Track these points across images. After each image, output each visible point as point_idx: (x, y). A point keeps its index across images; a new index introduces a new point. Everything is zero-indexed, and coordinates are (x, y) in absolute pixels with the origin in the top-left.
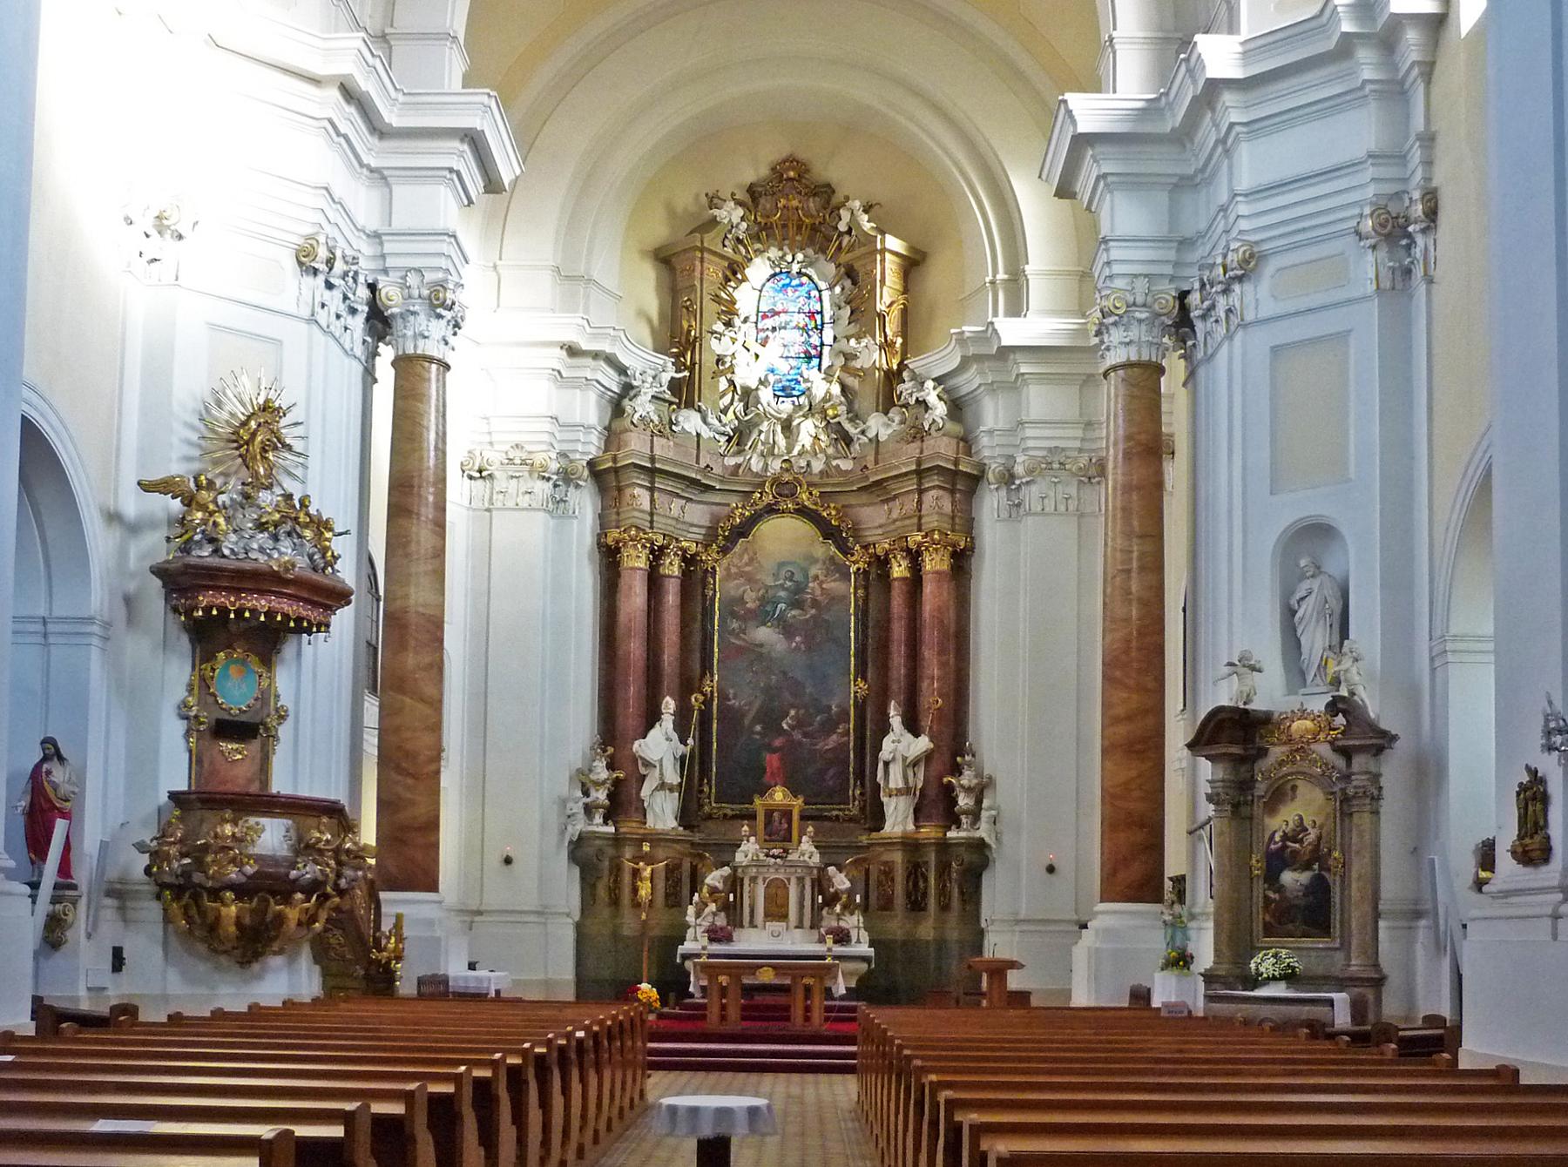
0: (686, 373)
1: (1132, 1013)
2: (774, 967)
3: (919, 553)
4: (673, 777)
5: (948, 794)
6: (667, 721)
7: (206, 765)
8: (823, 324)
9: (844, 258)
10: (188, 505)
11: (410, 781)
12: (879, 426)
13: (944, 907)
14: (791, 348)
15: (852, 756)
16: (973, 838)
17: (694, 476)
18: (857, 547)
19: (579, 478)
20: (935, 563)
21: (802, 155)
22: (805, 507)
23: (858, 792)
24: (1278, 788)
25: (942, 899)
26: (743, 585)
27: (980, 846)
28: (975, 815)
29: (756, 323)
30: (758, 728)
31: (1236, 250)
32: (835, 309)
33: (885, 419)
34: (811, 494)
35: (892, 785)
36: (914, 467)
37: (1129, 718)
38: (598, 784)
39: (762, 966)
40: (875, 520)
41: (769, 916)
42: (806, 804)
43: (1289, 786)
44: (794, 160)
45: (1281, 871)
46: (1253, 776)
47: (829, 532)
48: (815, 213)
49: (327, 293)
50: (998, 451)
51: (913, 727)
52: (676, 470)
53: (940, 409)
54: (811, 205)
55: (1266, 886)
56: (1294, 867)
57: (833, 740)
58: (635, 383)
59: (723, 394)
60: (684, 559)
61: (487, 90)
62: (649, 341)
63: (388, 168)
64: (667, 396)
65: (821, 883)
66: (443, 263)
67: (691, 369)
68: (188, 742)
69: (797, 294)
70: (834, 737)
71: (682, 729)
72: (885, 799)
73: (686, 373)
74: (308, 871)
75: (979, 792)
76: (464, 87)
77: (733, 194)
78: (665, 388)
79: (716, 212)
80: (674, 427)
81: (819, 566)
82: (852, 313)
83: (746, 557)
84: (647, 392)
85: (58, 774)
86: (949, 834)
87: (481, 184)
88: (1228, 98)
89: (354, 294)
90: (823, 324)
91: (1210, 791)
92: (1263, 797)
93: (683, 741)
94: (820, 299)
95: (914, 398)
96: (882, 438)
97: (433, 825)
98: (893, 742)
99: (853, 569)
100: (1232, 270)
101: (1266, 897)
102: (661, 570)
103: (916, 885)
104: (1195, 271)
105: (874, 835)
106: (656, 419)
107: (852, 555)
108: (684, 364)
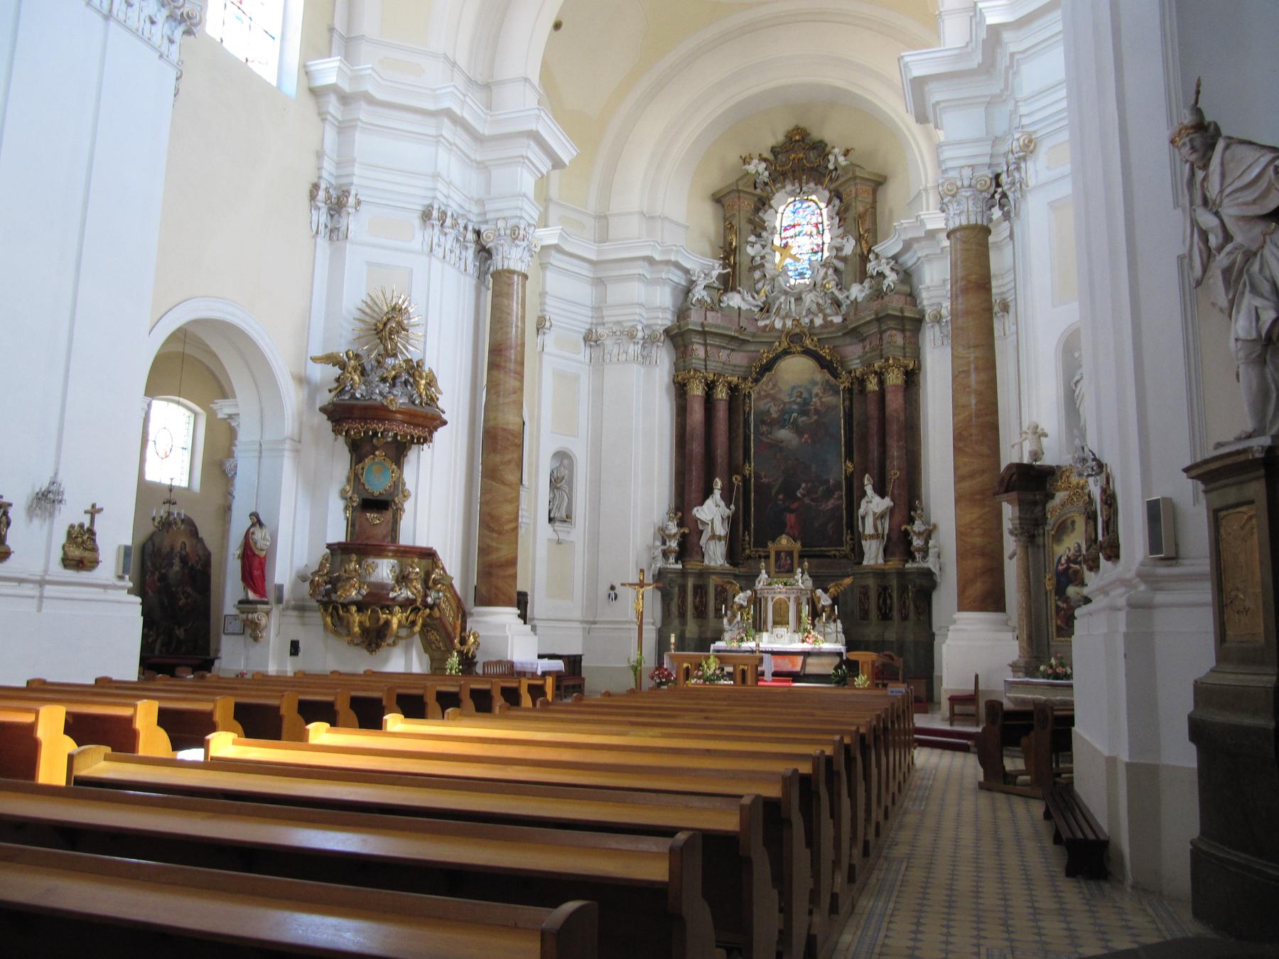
0: (729, 270)
1: (867, 692)
4: (721, 530)
5: (906, 538)
7: (357, 527)
8: (823, 230)
9: (833, 186)
11: (495, 535)
12: (857, 291)
13: (905, 618)
17: (733, 334)
18: (844, 373)
19: (658, 341)
20: (894, 378)
21: (802, 125)
24: (1060, 525)
25: (903, 611)
26: (769, 403)
27: (928, 574)
28: (925, 551)
30: (781, 497)
31: (1018, 139)
34: (812, 340)
35: (866, 532)
36: (873, 317)
37: (971, 476)
38: (671, 537)
40: (854, 354)
43: (1069, 522)
45: (1067, 585)
46: (1045, 515)
48: (813, 159)
49: (443, 239)
50: (933, 301)
51: (881, 492)
53: (891, 278)
55: (1057, 598)
56: (1077, 583)
57: (831, 504)
58: (694, 278)
59: (759, 281)
60: (730, 388)
63: (490, 160)
64: (715, 285)
65: (813, 603)
67: (734, 267)
68: (346, 513)
69: (806, 213)
70: (832, 501)
71: (727, 498)
73: (729, 270)
74: (406, 593)
75: (928, 535)
77: (760, 155)
78: (714, 279)
79: (747, 167)
81: (820, 386)
82: (840, 221)
85: (259, 535)
86: (907, 566)
87: (549, 164)
88: (1007, 36)
90: (823, 230)
93: (728, 506)
94: (821, 214)
96: (859, 300)
99: (842, 386)
100: (1017, 153)
101: (1057, 607)
102: (715, 397)
103: (885, 601)
105: (856, 567)
106: (709, 300)
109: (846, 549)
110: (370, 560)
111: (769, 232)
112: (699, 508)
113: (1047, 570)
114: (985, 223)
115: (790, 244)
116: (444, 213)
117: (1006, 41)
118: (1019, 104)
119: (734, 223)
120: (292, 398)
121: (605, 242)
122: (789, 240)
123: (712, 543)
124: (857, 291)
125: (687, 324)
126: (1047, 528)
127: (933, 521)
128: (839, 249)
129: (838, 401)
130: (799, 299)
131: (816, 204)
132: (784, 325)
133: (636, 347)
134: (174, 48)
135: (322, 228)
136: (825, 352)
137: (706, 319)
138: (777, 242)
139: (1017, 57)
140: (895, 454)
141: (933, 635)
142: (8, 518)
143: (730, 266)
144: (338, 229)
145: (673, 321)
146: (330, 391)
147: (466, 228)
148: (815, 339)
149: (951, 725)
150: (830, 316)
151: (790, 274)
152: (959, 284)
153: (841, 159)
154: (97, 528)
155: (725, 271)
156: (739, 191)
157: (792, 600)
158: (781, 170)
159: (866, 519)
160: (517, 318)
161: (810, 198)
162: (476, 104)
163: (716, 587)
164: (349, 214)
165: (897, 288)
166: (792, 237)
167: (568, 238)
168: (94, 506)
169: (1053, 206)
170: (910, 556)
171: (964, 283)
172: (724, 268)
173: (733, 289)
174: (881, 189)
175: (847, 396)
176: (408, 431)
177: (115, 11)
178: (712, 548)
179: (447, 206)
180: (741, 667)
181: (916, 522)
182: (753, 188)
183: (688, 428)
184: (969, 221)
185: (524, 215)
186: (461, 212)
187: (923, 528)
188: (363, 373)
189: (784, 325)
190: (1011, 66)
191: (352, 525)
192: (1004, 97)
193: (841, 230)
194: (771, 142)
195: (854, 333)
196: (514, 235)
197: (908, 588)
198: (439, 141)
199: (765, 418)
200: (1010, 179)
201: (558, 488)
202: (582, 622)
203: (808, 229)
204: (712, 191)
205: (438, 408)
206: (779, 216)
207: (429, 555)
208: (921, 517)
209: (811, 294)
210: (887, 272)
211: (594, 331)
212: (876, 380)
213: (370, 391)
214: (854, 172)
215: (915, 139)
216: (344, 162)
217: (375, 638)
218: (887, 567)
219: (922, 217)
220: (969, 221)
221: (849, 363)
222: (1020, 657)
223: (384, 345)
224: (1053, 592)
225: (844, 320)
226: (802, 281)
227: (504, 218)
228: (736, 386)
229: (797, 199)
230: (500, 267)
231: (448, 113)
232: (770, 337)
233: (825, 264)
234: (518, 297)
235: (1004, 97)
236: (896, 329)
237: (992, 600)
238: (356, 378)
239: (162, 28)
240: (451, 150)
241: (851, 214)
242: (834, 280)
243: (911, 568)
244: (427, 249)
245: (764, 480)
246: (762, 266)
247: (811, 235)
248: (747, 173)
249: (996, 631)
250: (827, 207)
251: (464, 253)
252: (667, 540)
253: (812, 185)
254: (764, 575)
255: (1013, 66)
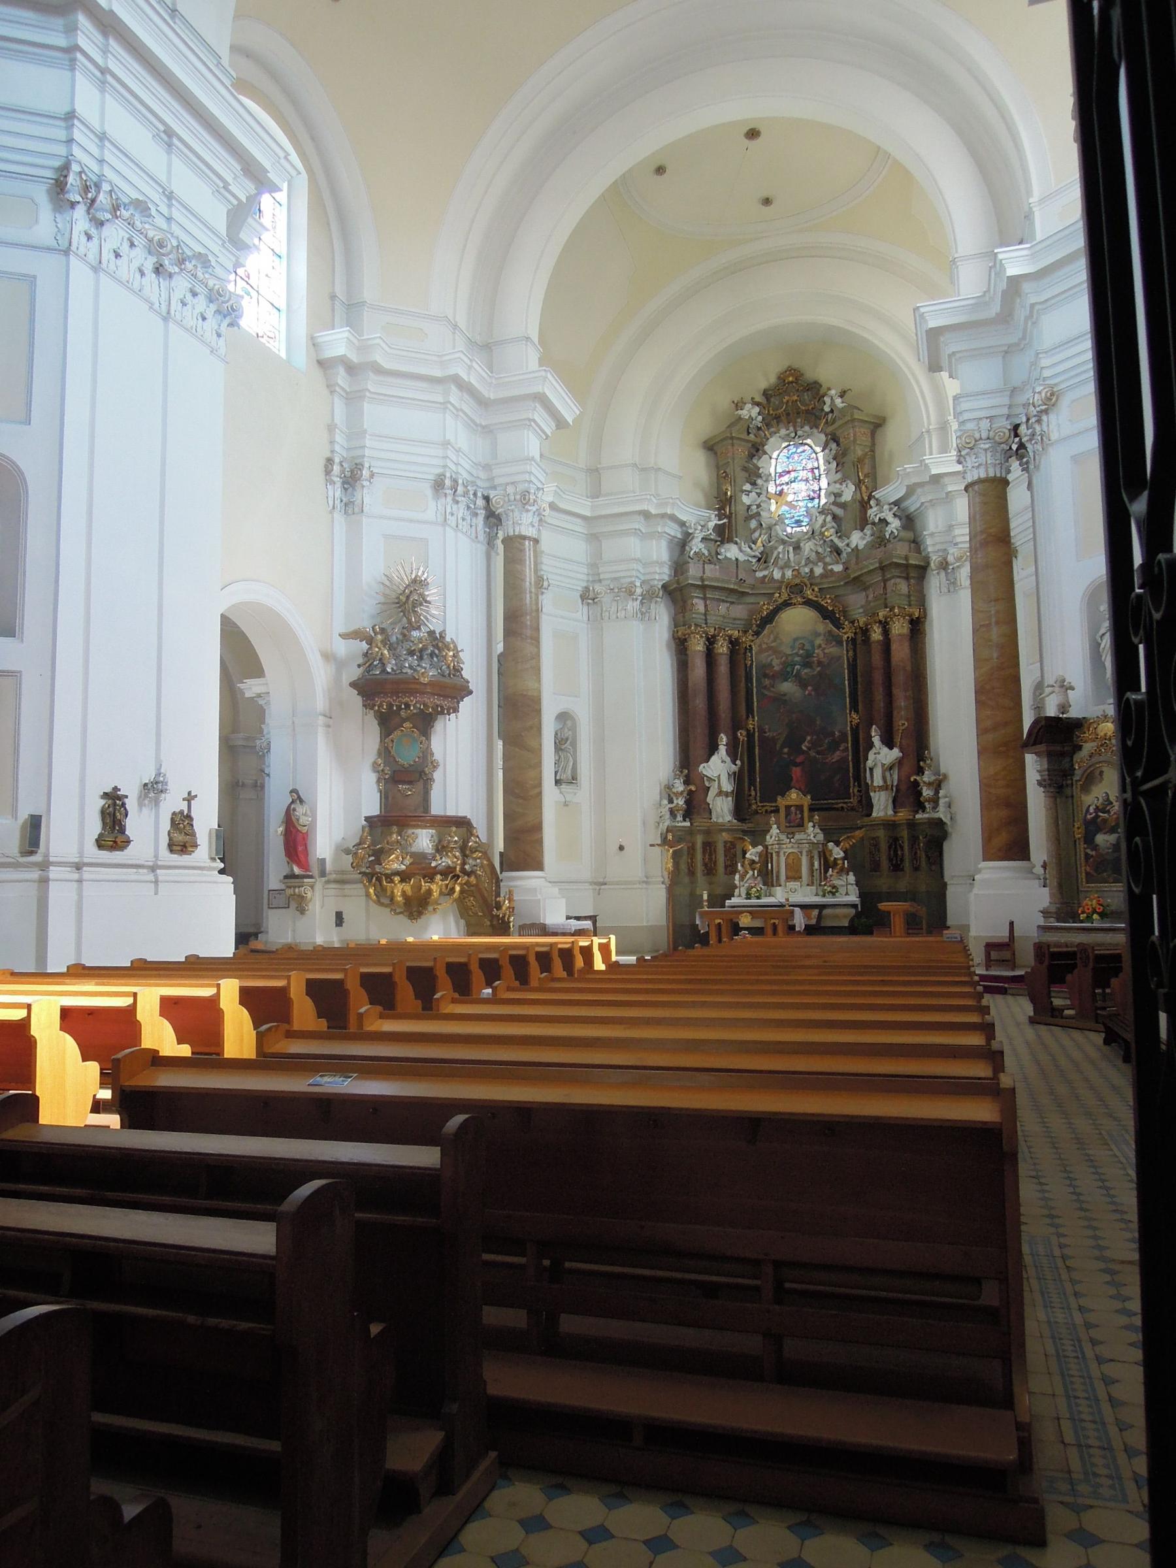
0: (725, 521)
2: (750, 912)
3: (887, 623)
4: (728, 786)
6: (722, 749)
7: (390, 799)
8: (820, 476)
9: (830, 429)
10: (370, 644)
11: (521, 801)
12: (858, 539)
14: (800, 495)
15: (851, 766)
16: (933, 819)
17: (732, 587)
18: (846, 623)
19: (657, 597)
20: (899, 628)
21: (795, 366)
22: (811, 600)
23: (856, 790)
24: (1088, 775)
26: (769, 656)
27: (940, 823)
28: (935, 801)
29: (775, 481)
30: (786, 750)
31: (1040, 393)
32: (827, 464)
33: (861, 534)
34: (813, 590)
35: (875, 784)
36: (877, 565)
39: (742, 912)
40: (856, 603)
41: (788, 878)
42: (812, 800)
44: (792, 369)
45: (1095, 835)
46: (1073, 765)
47: (826, 614)
48: (808, 402)
49: (455, 507)
50: (938, 547)
51: (889, 743)
52: (719, 585)
53: (895, 524)
54: (806, 397)
55: (1085, 846)
57: (837, 756)
58: (690, 531)
59: (754, 531)
60: (731, 642)
61: (544, 368)
62: (703, 503)
63: (496, 424)
64: (712, 537)
65: (824, 855)
66: (527, 477)
67: (729, 517)
68: (379, 785)
69: (801, 458)
70: (838, 753)
71: (733, 754)
72: (872, 794)
73: (725, 521)
74: (445, 861)
75: (938, 785)
76: (540, 365)
77: (752, 398)
78: (711, 531)
79: (740, 412)
80: (719, 557)
81: (822, 637)
82: (837, 465)
83: (772, 636)
84: (699, 536)
85: (300, 810)
87: (553, 425)
88: (1027, 287)
89: (475, 504)
90: (820, 476)
91: (1039, 778)
92: (1080, 780)
94: (817, 459)
95: (878, 518)
96: (861, 547)
97: (538, 828)
98: (875, 754)
100: (1039, 406)
101: (1086, 854)
102: (716, 651)
103: (896, 851)
104: (1021, 410)
105: (866, 819)
106: (706, 553)
107: (843, 629)
108: (724, 514)
109: (854, 801)
110: (410, 831)
111: (764, 479)
112: (705, 764)
113: (1076, 819)
114: (1004, 475)
115: (785, 491)
116: (455, 481)
117: (1026, 291)
118: (1041, 356)
119: (727, 471)
120: (321, 675)
121: (598, 498)
122: (784, 487)
123: (719, 800)
124: (858, 539)
125: (687, 579)
126: (1075, 778)
127: (943, 770)
128: (838, 495)
129: (842, 653)
130: (797, 548)
131: (811, 447)
132: (783, 575)
133: (635, 604)
134: (221, 341)
135: (338, 502)
136: (827, 602)
137: (704, 573)
138: (772, 489)
139: (1037, 307)
140: (903, 704)
141: (945, 885)
142: (125, 809)
143: (726, 517)
144: (353, 503)
145: (670, 576)
146: (359, 666)
147: (475, 494)
148: (816, 589)
149: (987, 970)
150: (831, 565)
151: (787, 522)
152: (979, 538)
153: (838, 401)
154: (193, 814)
155: (722, 522)
156: (732, 438)
157: (804, 853)
158: (774, 413)
159: (874, 770)
160: (530, 583)
161: (805, 441)
162: (483, 369)
163: (726, 842)
164: (363, 486)
165: (901, 534)
166: (787, 483)
167: (564, 496)
168: (189, 793)
169: (1075, 459)
170: (920, 807)
171: (983, 537)
172: (719, 520)
173: (730, 540)
174: (879, 431)
175: (850, 646)
176: (438, 703)
177: (172, 312)
178: (719, 804)
179: (457, 473)
180: (772, 921)
181: (926, 772)
182: (746, 433)
183: (690, 684)
184: (987, 474)
185: (533, 479)
186: (470, 478)
187: (933, 778)
188: (391, 648)
189: (783, 575)
190: (1031, 316)
191: (385, 797)
192: (1022, 346)
193: (839, 476)
194: (763, 385)
195: (857, 582)
196: (524, 500)
197: (919, 839)
198: (447, 408)
199: (767, 672)
200: (1030, 431)
201: (561, 749)
202: (591, 883)
203: (803, 474)
204: (704, 438)
205: (462, 678)
206: (773, 461)
207: (463, 823)
208: (930, 766)
209: (810, 543)
210: (890, 518)
211: (591, 588)
212: (880, 629)
213: (399, 665)
214: (852, 414)
215: (917, 382)
216: (356, 433)
217: (416, 907)
218: (896, 818)
219: (927, 461)
220: (987, 474)
221: (850, 613)
222: (1050, 903)
223: (408, 618)
224: (1082, 839)
225: (846, 569)
226: (798, 529)
227: (512, 483)
228: (737, 639)
229: (791, 443)
230: (511, 533)
231: (456, 380)
232: (770, 588)
233: (823, 511)
234: (530, 562)
235: (1022, 346)
236: (899, 577)
237: (1017, 849)
238: (386, 652)
239: (211, 323)
240: (457, 416)
241: (851, 457)
242: (833, 527)
243: (921, 819)
244: (440, 519)
245: (768, 734)
246: (758, 514)
247: (807, 480)
248: (740, 418)
249: (1025, 879)
250: (822, 451)
251: (474, 519)
252: (674, 798)
253: (807, 428)
254: (774, 830)
255: (1033, 316)
